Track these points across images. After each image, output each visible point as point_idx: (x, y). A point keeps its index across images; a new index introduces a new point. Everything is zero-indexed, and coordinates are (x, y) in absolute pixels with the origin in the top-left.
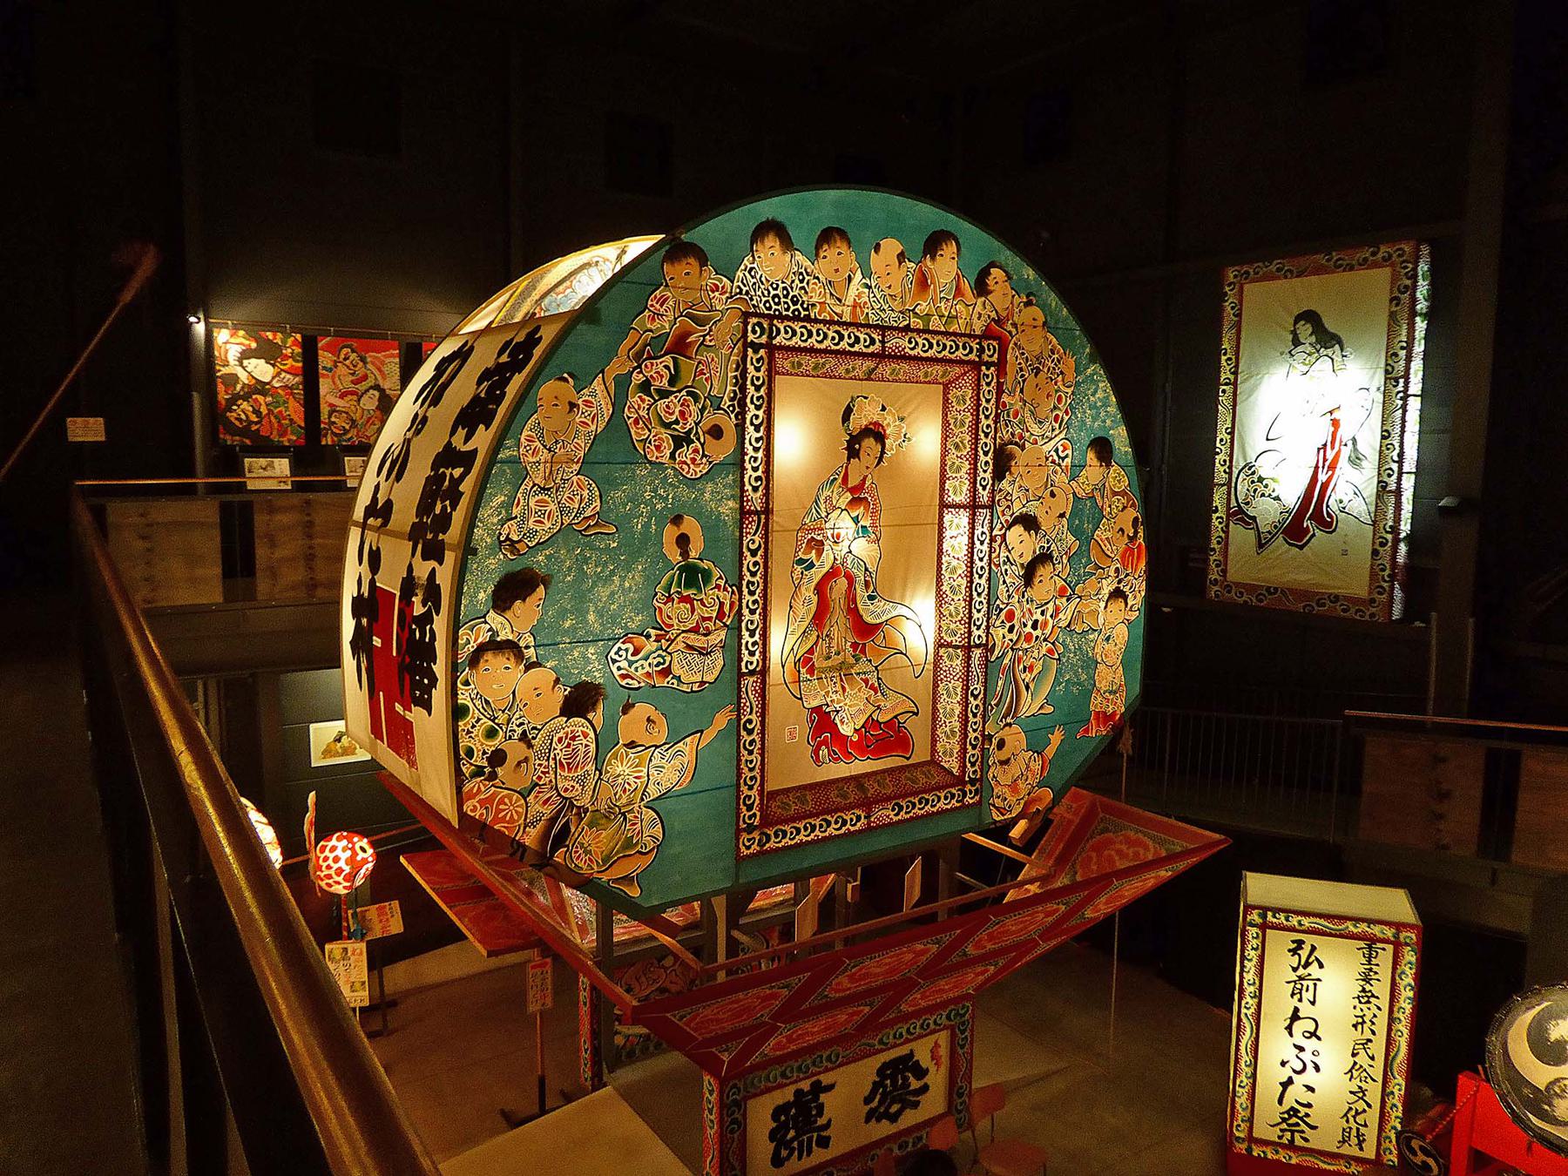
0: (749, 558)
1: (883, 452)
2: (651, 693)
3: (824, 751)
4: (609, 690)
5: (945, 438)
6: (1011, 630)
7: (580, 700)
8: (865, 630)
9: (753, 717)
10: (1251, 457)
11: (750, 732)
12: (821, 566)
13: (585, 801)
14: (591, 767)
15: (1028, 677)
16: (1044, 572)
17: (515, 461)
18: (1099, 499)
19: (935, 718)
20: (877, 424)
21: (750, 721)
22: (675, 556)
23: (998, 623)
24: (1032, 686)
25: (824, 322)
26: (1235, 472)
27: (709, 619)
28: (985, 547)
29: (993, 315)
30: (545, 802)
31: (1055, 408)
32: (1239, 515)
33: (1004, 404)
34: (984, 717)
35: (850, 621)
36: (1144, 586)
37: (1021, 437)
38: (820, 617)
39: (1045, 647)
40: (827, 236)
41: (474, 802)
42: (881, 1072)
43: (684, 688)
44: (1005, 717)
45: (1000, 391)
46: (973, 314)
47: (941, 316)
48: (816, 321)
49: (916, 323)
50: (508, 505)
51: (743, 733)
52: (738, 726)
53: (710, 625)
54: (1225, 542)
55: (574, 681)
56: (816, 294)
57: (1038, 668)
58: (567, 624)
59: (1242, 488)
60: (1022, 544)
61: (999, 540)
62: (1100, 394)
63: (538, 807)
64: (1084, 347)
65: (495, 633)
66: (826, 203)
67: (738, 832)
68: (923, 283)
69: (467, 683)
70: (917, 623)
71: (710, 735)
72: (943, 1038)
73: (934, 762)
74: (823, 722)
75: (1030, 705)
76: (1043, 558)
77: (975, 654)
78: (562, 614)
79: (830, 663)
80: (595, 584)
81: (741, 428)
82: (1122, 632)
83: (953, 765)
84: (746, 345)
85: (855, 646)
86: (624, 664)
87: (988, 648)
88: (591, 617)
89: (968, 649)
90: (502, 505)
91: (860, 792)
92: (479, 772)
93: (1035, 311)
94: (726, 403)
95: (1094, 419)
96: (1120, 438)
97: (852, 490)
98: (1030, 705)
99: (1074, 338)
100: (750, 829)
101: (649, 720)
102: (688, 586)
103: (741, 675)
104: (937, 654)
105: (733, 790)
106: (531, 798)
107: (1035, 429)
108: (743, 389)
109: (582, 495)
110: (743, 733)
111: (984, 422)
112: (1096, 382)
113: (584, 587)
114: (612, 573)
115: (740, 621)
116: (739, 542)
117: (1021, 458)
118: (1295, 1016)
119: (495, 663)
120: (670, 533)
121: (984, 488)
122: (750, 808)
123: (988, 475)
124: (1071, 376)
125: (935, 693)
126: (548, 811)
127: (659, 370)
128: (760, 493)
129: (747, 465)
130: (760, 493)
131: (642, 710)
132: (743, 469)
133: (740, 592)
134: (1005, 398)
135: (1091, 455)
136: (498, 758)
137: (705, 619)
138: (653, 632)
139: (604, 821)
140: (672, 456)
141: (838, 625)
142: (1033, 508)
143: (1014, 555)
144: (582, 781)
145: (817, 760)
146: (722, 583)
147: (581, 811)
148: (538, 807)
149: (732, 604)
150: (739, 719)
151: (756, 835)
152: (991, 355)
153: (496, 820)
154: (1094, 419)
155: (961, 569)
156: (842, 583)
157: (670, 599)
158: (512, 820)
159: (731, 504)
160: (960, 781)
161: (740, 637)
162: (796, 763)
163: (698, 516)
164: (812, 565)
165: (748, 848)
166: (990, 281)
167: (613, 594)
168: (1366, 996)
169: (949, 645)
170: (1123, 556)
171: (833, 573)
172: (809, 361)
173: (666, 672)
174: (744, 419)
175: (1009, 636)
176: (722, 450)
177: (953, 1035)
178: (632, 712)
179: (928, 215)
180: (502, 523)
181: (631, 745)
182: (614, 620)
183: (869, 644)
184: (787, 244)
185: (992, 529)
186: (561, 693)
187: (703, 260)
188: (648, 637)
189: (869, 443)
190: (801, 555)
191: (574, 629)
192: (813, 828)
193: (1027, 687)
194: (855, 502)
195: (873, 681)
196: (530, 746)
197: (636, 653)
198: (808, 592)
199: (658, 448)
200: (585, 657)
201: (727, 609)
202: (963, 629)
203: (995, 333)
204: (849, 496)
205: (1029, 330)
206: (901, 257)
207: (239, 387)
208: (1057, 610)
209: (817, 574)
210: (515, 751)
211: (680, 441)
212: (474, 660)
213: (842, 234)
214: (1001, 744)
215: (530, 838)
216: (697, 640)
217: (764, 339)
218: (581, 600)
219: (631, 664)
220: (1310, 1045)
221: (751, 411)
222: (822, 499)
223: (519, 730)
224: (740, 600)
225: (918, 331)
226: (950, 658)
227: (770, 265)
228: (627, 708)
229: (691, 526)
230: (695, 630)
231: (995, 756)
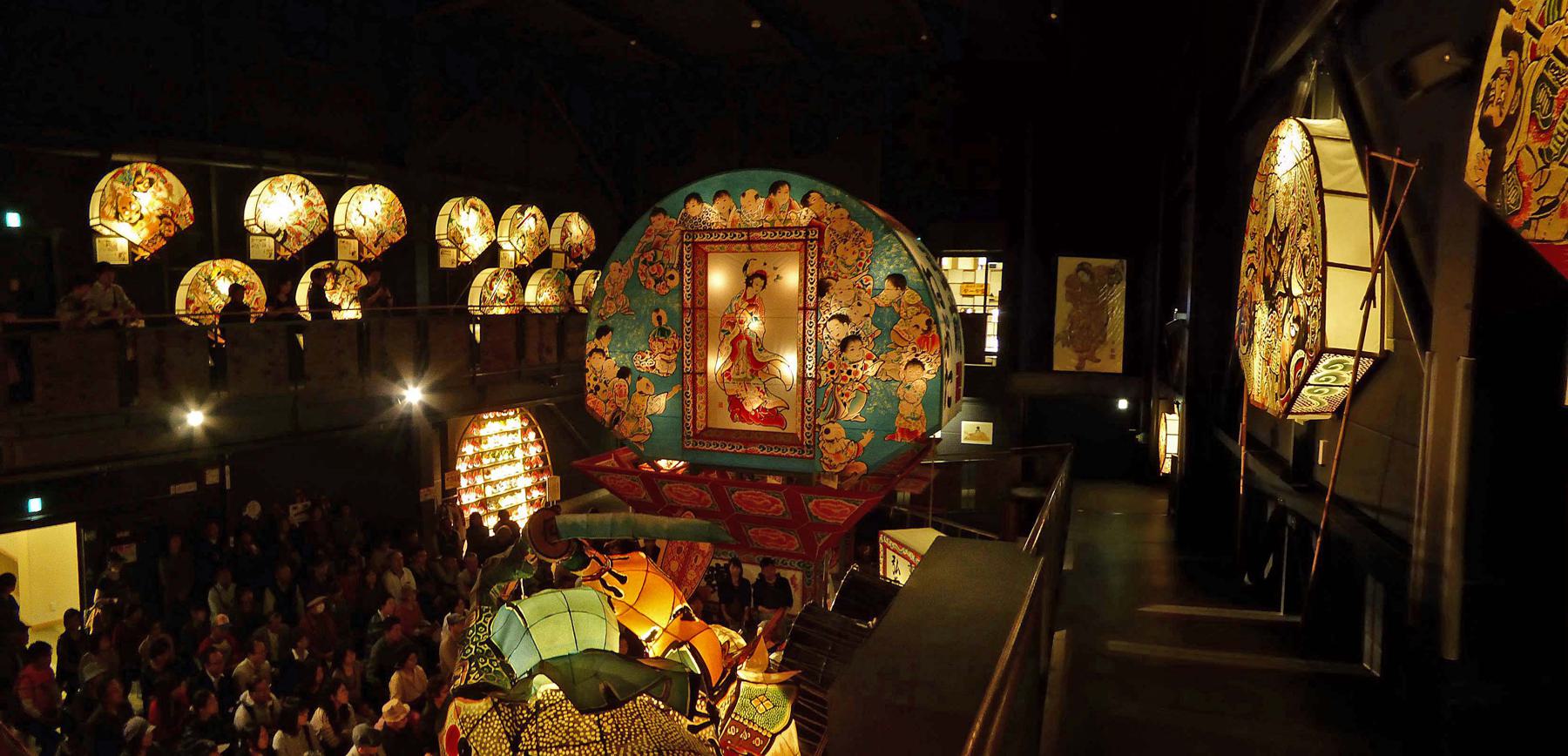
7: (624, 373)
15: (845, 399)
16: (855, 345)
22: (656, 324)
35: (753, 361)
39: (857, 386)
40: (718, 195)
45: (820, 252)
49: (766, 225)
57: (853, 395)
66: (717, 181)
70: (788, 366)
71: (672, 394)
74: (736, 404)
87: (817, 381)
91: (748, 438)
93: (841, 210)
98: (851, 413)
107: (845, 270)
109: (623, 300)
116: (692, 322)
117: (835, 286)
119: (597, 356)
120: (654, 315)
127: (649, 255)
131: (645, 380)
135: (888, 284)
141: (743, 362)
142: (844, 311)
145: (732, 417)
152: (814, 234)
156: (745, 342)
166: (811, 200)
170: (919, 341)
171: (740, 337)
172: (717, 247)
176: (674, 283)
179: (773, 175)
184: (700, 201)
187: (665, 214)
189: (758, 280)
194: (750, 306)
198: (727, 344)
203: (816, 224)
206: (757, 197)
208: (865, 367)
210: (603, 387)
211: (658, 281)
213: (726, 192)
214: (827, 431)
227: (694, 209)
229: (662, 313)
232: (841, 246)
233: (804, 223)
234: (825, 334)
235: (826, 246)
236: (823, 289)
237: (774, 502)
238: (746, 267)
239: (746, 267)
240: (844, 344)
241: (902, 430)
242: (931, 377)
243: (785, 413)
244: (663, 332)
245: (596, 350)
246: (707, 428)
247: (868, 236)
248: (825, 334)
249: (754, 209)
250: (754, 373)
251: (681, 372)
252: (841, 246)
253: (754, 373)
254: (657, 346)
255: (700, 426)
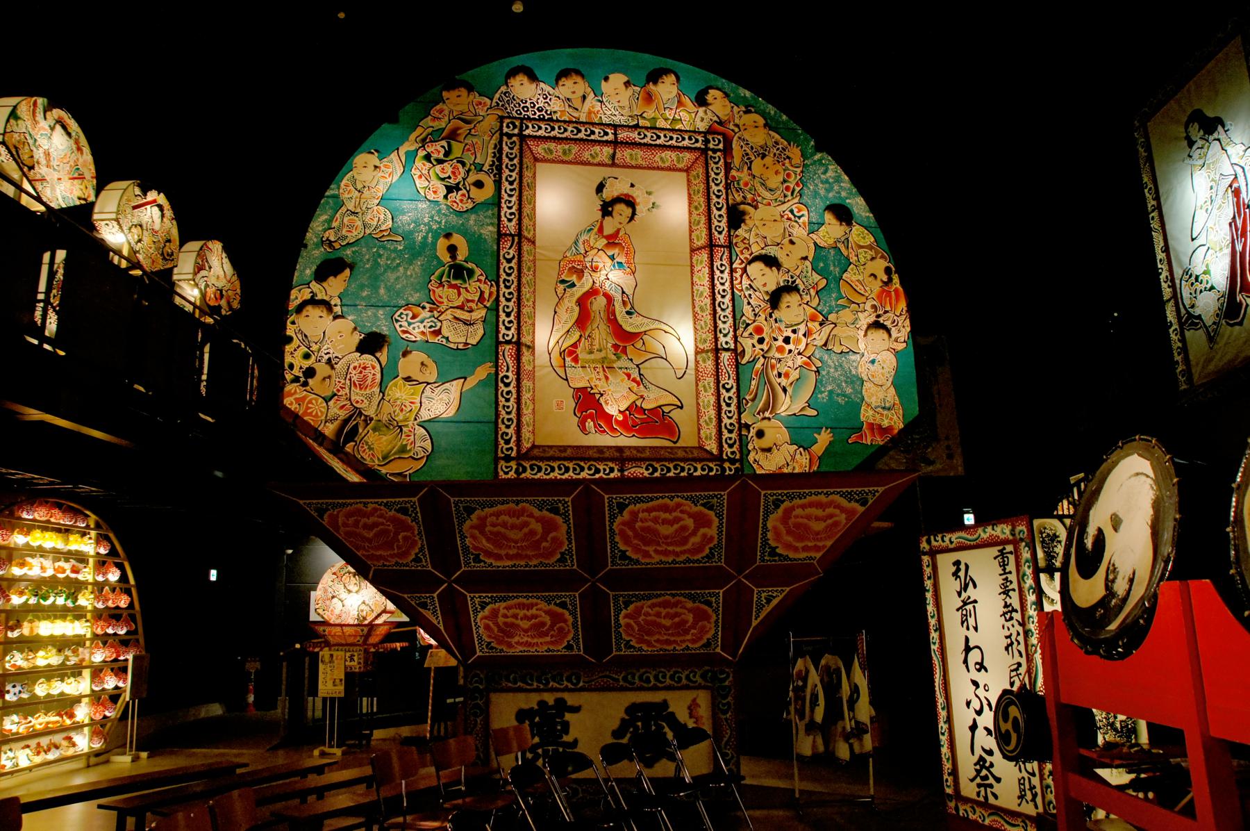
0: (505, 264)
1: (634, 214)
2: (426, 346)
3: (590, 424)
4: (392, 340)
5: (690, 204)
6: (761, 341)
7: (371, 343)
8: (625, 339)
9: (510, 374)
10: (1186, 265)
11: (507, 385)
12: (582, 286)
13: (371, 412)
14: (377, 390)
15: (784, 381)
16: (790, 299)
17: (336, 197)
18: (843, 249)
19: (698, 411)
20: (627, 195)
21: (507, 377)
22: (446, 258)
23: (746, 334)
24: (790, 390)
25: (565, 122)
26: (1177, 282)
27: (473, 301)
28: (726, 275)
29: (715, 119)
30: (342, 407)
31: (785, 181)
32: (1190, 320)
33: (734, 177)
34: (739, 407)
36: (908, 322)
37: (754, 200)
38: (583, 320)
39: (800, 360)
40: (564, 74)
41: (292, 399)
42: (632, 709)
43: (452, 346)
44: (764, 410)
45: (728, 168)
46: (698, 119)
47: (666, 119)
48: (558, 121)
50: (330, 221)
51: (501, 385)
52: (496, 379)
53: (473, 305)
54: (1184, 349)
55: (367, 330)
56: (556, 106)
57: (794, 375)
58: (364, 294)
59: (1186, 293)
60: (769, 279)
61: (740, 272)
62: (830, 174)
63: (336, 410)
64: (809, 143)
65: (314, 294)
66: (564, 57)
67: (496, 460)
68: (649, 98)
69: (293, 323)
71: (472, 382)
72: (703, 698)
73: (701, 448)
74: (587, 403)
75: (787, 406)
76: (790, 288)
77: (733, 365)
78: (362, 287)
79: (592, 357)
80: (385, 271)
81: (498, 183)
82: (889, 361)
83: (712, 446)
84: (502, 135)
85: (615, 347)
86: (406, 324)
87: (738, 353)
88: (382, 291)
89: (717, 351)
90: (325, 221)
91: (621, 456)
92: (296, 379)
94: (486, 168)
95: (828, 191)
96: (858, 205)
97: (607, 237)
98: (787, 406)
99: (799, 135)
100: (508, 459)
101: (422, 364)
102: (455, 277)
103: (498, 343)
104: (697, 362)
105: (492, 426)
106: (331, 403)
108: (500, 159)
110: (501, 385)
111: (714, 188)
112: (826, 166)
113: (378, 272)
114: (399, 265)
115: (498, 305)
118: (968, 649)
120: (442, 244)
121: (720, 233)
122: (507, 442)
123: (724, 224)
124: (797, 159)
125: (697, 389)
126: (343, 414)
128: (514, 223)
129: (503, 205)
130: (514, 223)
131: (417, 356)
132: (500, 207)
133: (498, 286)
134: (733, 173)
135: (829, 217)
136: (310, 372)
137: (468, 301)
138: (428, 306)
139: (384, 429)
140: (446, 197)
141: (601, 334)
142: (772, 251)
143: (756, 284)
144: (370, 398)
145: (583, 429)
146: (483, 278)
147: (367, 420)
148: (336, 410)
149: (491, 294)
150: (497, 374)
151: (513, 464)
153: (305, 413)
154: (828, 191)
155: (707, 292)
157: (441, 285)
158: (317, 415)
159: (490, 228)
160: (719, 459)
161: (498, 316)
162: (552, 419)
163: (464, 233)
164: (573, 285)
165: (506, 473)
166: (709, 98)
167: (398, 278)
168: (1008, 611)
169: (703, 351)
170: (879, 297)
171: (593, 292)
173: (438, 333)
174: (501, 178)
175: (758, 346)
177: (713, 699)
178: (410, 357)
180: (325, 231)
181: (408, 379)
182: (398, 294)
183: (629, 349)
184: (533, 78)
185: (731, 264)
186: (357, 338)
187: (470, 89)
188: (424, 308)
189: (620, 208)
190: (563, 277)
191: (369, 297)
192: (567, 470)
193: (785, 390)
195: (635, 375)
196: (333, 368)
197: (413, 318)
199: (435, 192)
200: (375, 315)
201: (486, 296)
202: (711, 336)
203: (717, 129)
204: (605, 242)
205: (752, 130)
206: (627, 84)
207: (103, 551)
209: (578, 292)
212: (299, 309)
213: (578, 73)
214: (760, 434)
215: (329, 430)
216: (464, 315)
217: (516, 131)
218: (375, 280)
219: (409, 324)
220: (981, 677)
221: (506, 173)
222: (581, 241)
223: (326, 357)
224: (498, 291)
225: (646, 128)
226: (704, 361)
227: (523, 89)
228: (405, 354)
229: (458, 240)
230: (461, 307)
231: (754, 444)
232: (757, 164)
233: (702, 127)
234: (746, 282)
235: (737, 161)
236: (736, 218)
237: (701, 521)
238: (600, 188)
239: (600, 188)
240: (775, 299)
241: (871, 426)
242: (901, 347)
243: (676, 415)
244: (459, 272)
245: (313, 302)
246: (534, 446)
247: (795, 153)
248: (746, 282)
249: (614, 100)
250: (619, 350)
251: (494, 343)
252: (757, 164)
253: (619, 350)
254: (446, 294)
255: (526, 445)
